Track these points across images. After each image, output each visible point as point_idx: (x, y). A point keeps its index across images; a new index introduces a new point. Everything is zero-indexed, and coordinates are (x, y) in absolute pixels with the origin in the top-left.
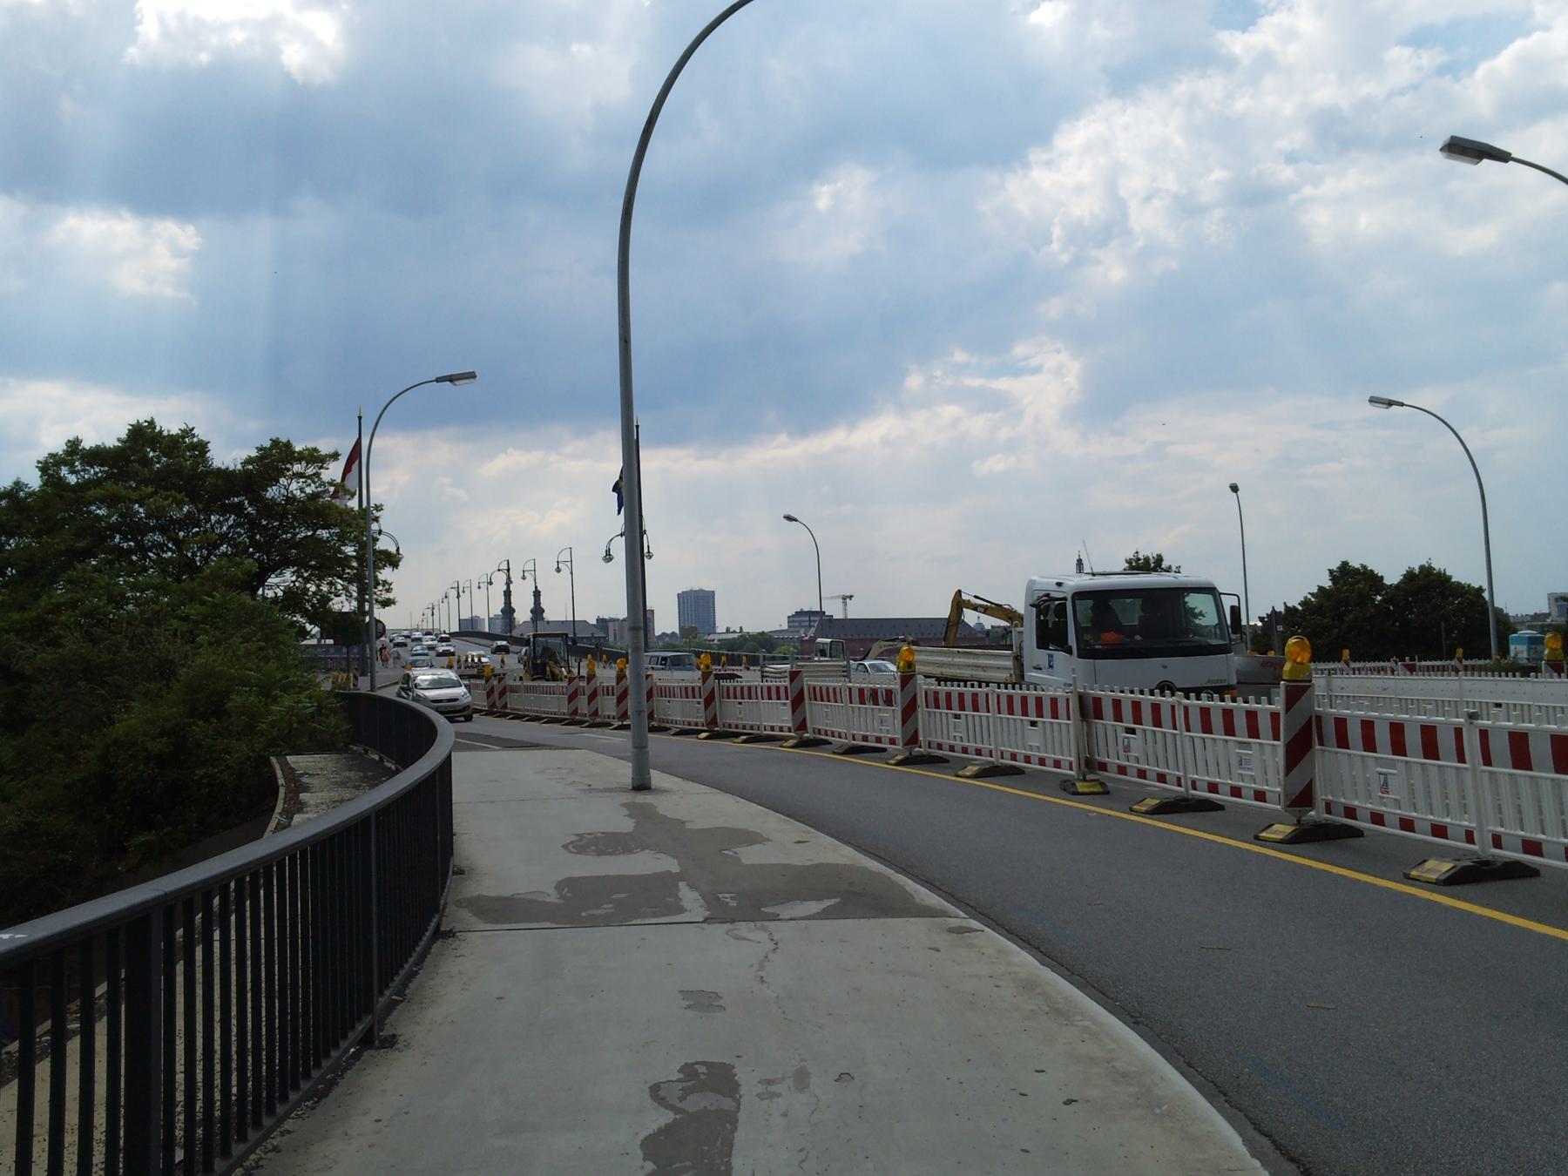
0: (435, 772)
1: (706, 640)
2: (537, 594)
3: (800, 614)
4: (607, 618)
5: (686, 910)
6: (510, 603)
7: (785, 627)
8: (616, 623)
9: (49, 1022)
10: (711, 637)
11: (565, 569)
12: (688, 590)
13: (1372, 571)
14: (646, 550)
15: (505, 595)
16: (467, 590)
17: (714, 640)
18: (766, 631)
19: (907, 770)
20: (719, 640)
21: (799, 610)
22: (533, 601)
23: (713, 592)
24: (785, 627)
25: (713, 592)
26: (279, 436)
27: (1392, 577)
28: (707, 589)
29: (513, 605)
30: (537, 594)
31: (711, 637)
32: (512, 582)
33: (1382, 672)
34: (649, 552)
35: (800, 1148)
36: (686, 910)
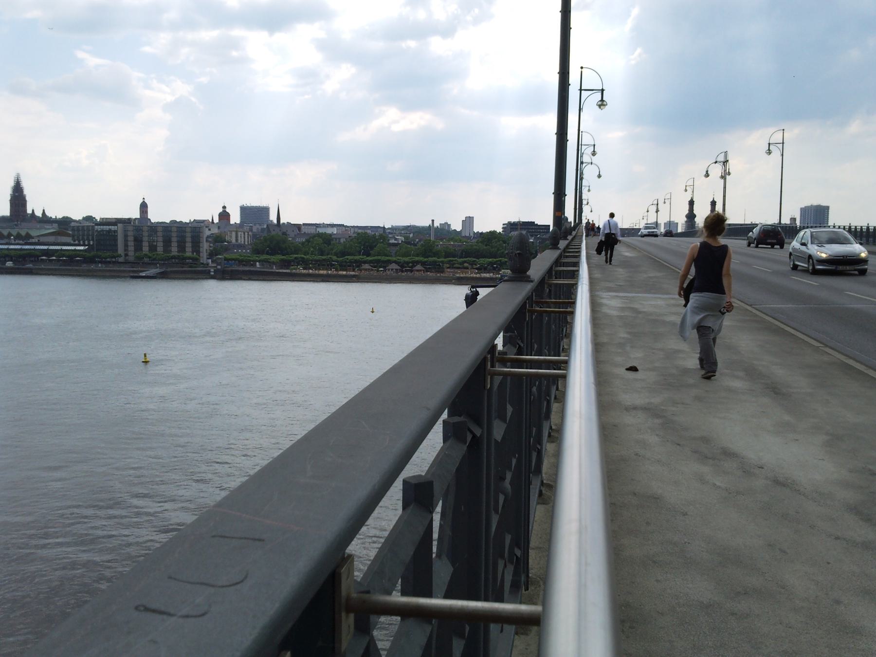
2: (691, 203)
5: (144, 201)
6: (693, 210)
12: (809, 205)
13: (490, 231)
14: (727, 171)
18: (484, 232)
19: (759, 251)
22: (688, 208)
23: (827, 208)
25: (827, 208)
26: (392, 224)
27: (499, 230)
28: (823, 205)
29: (694, 212)
30: (691, 203)
32: (729, 174)
33: (81, 228)
34: (729, 172)
36: (144, 201)
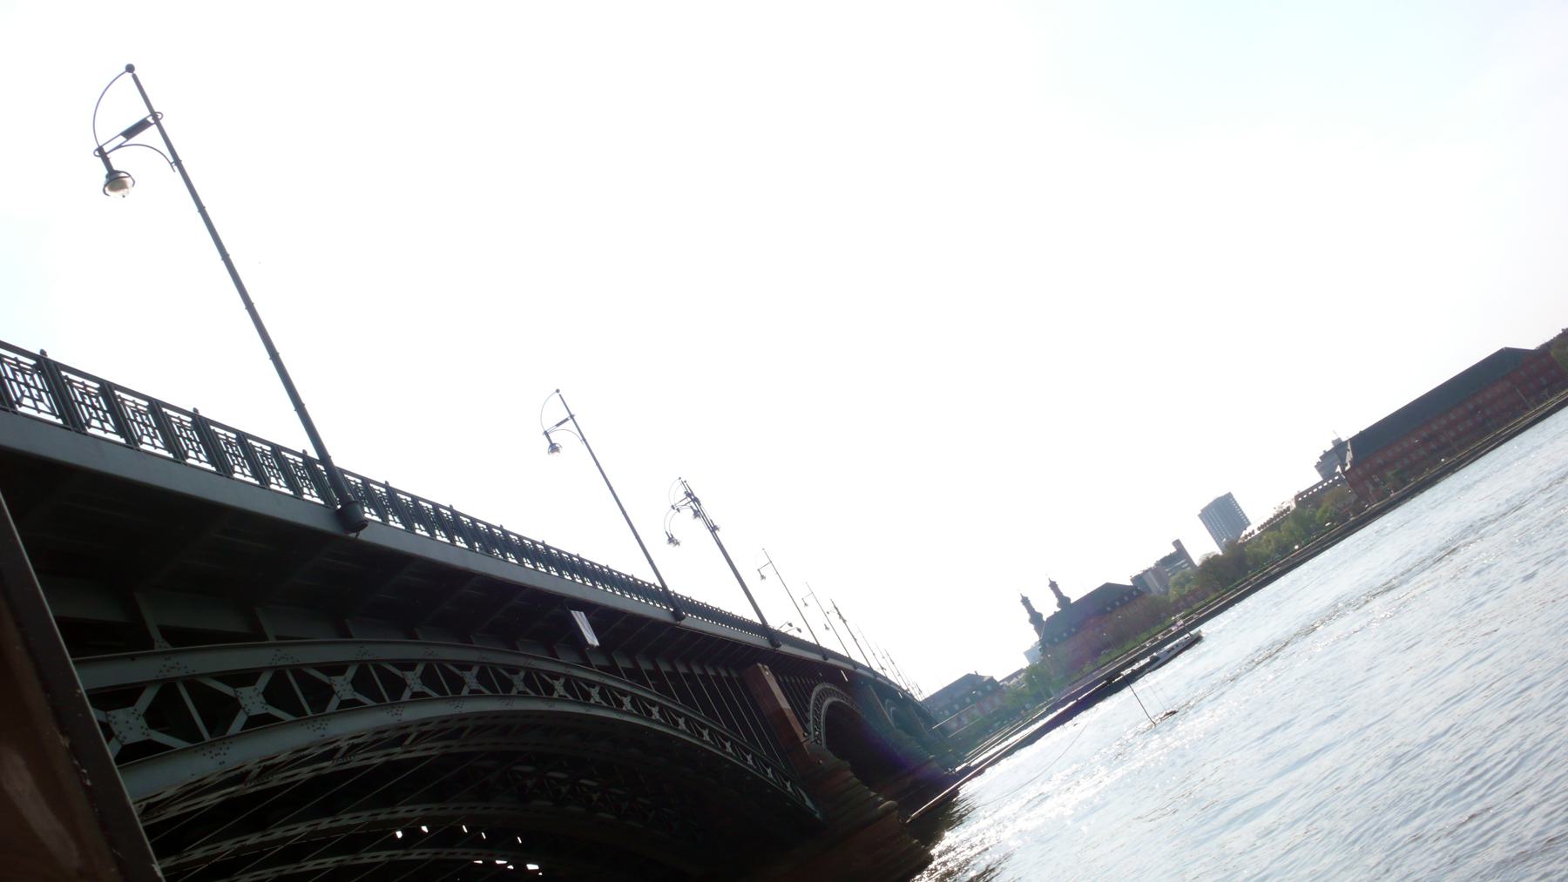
0: (701, 635)
1: (1246, 537)
3: (1326, 456)
4: (1140, 573)
7: (1319, 478)
8: (1149, 573)
9: (596, 643)
10: (1249, 530)
11: (767, 572)
15: (1024, 604)
16: (810, 601)
17: (1253, 532)
20: (1259, 529)
21: (1322, 454)
23: (1229, 496)
24: (1319, 478)
25: (1229, 496)
26: (1027, 621)
31: (1249, 530)
35: (1202, 778)
